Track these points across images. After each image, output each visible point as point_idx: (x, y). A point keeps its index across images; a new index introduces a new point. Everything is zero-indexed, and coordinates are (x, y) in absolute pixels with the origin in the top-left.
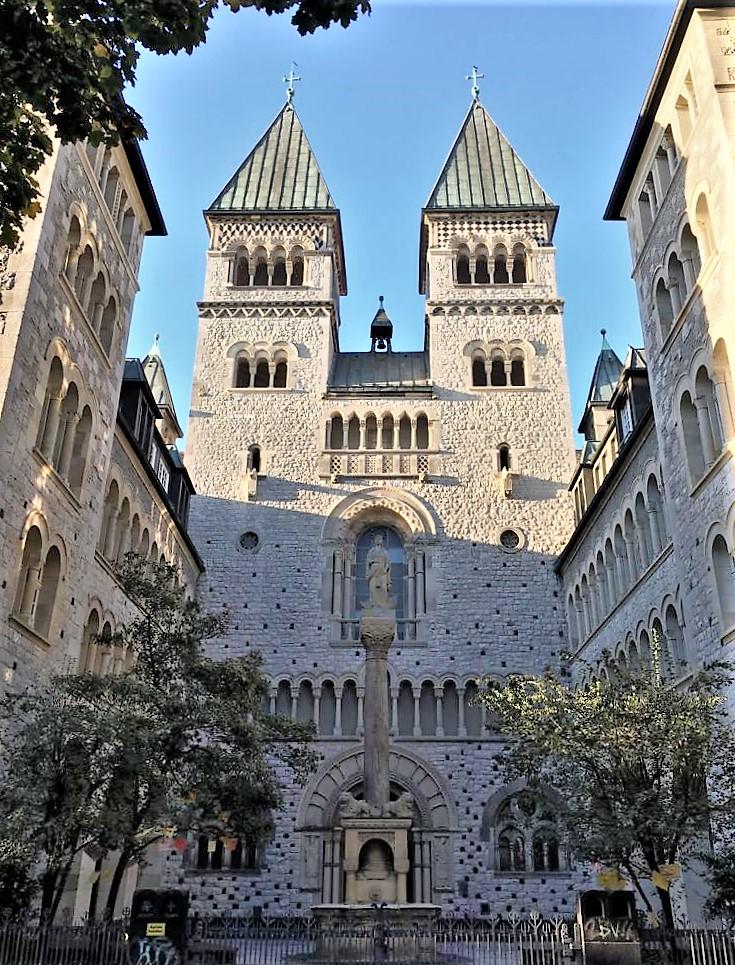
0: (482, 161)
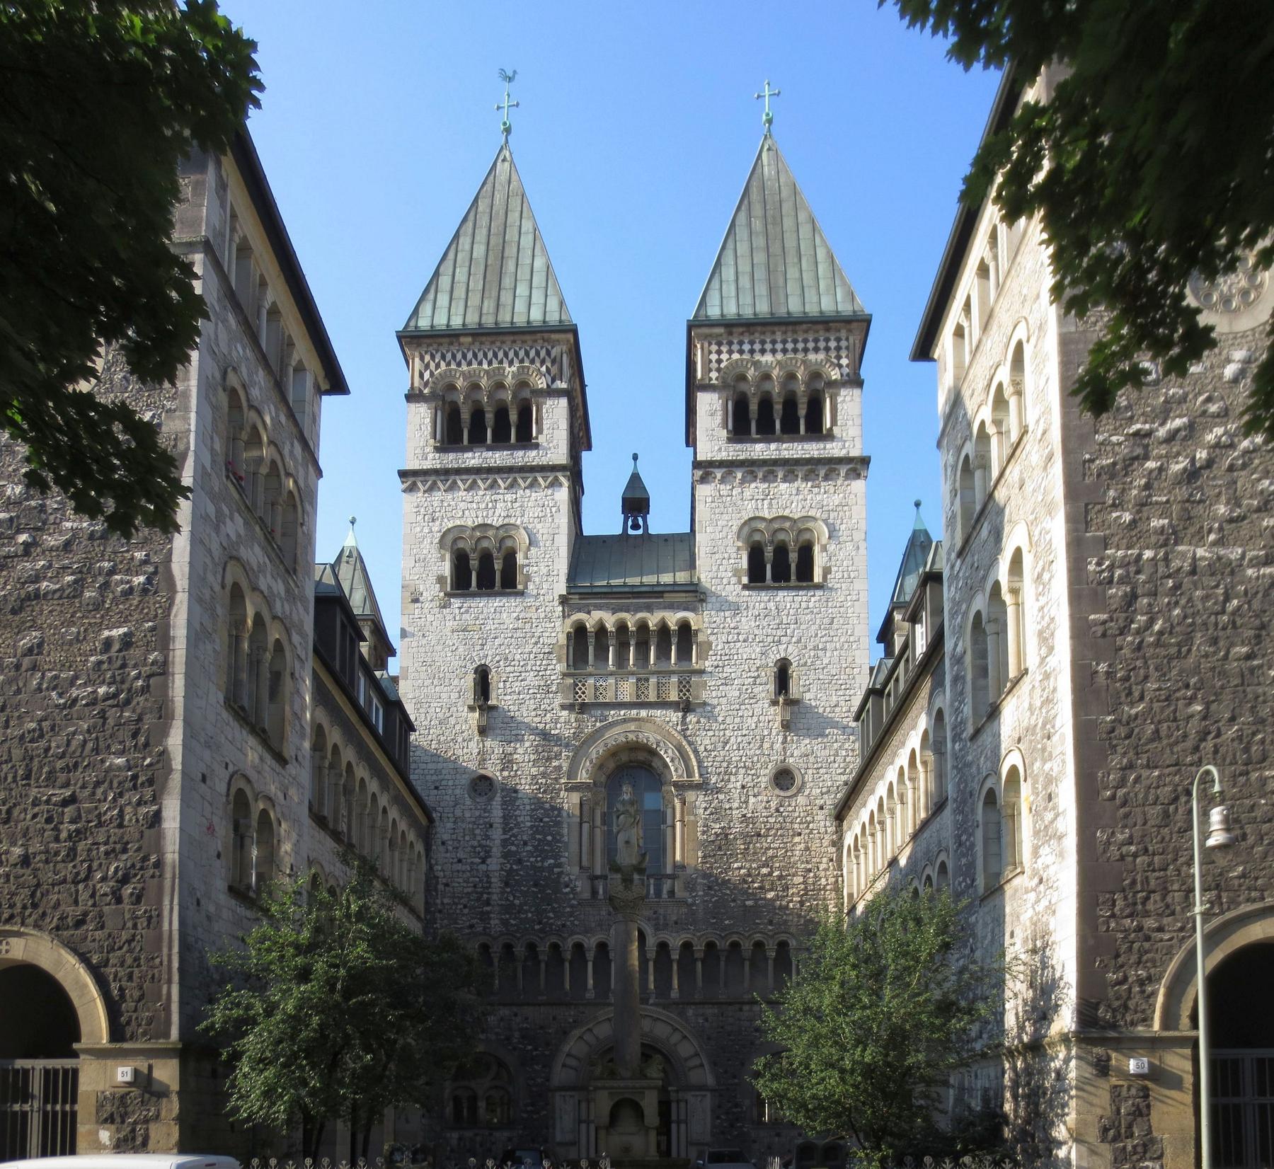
0: (770, 242)
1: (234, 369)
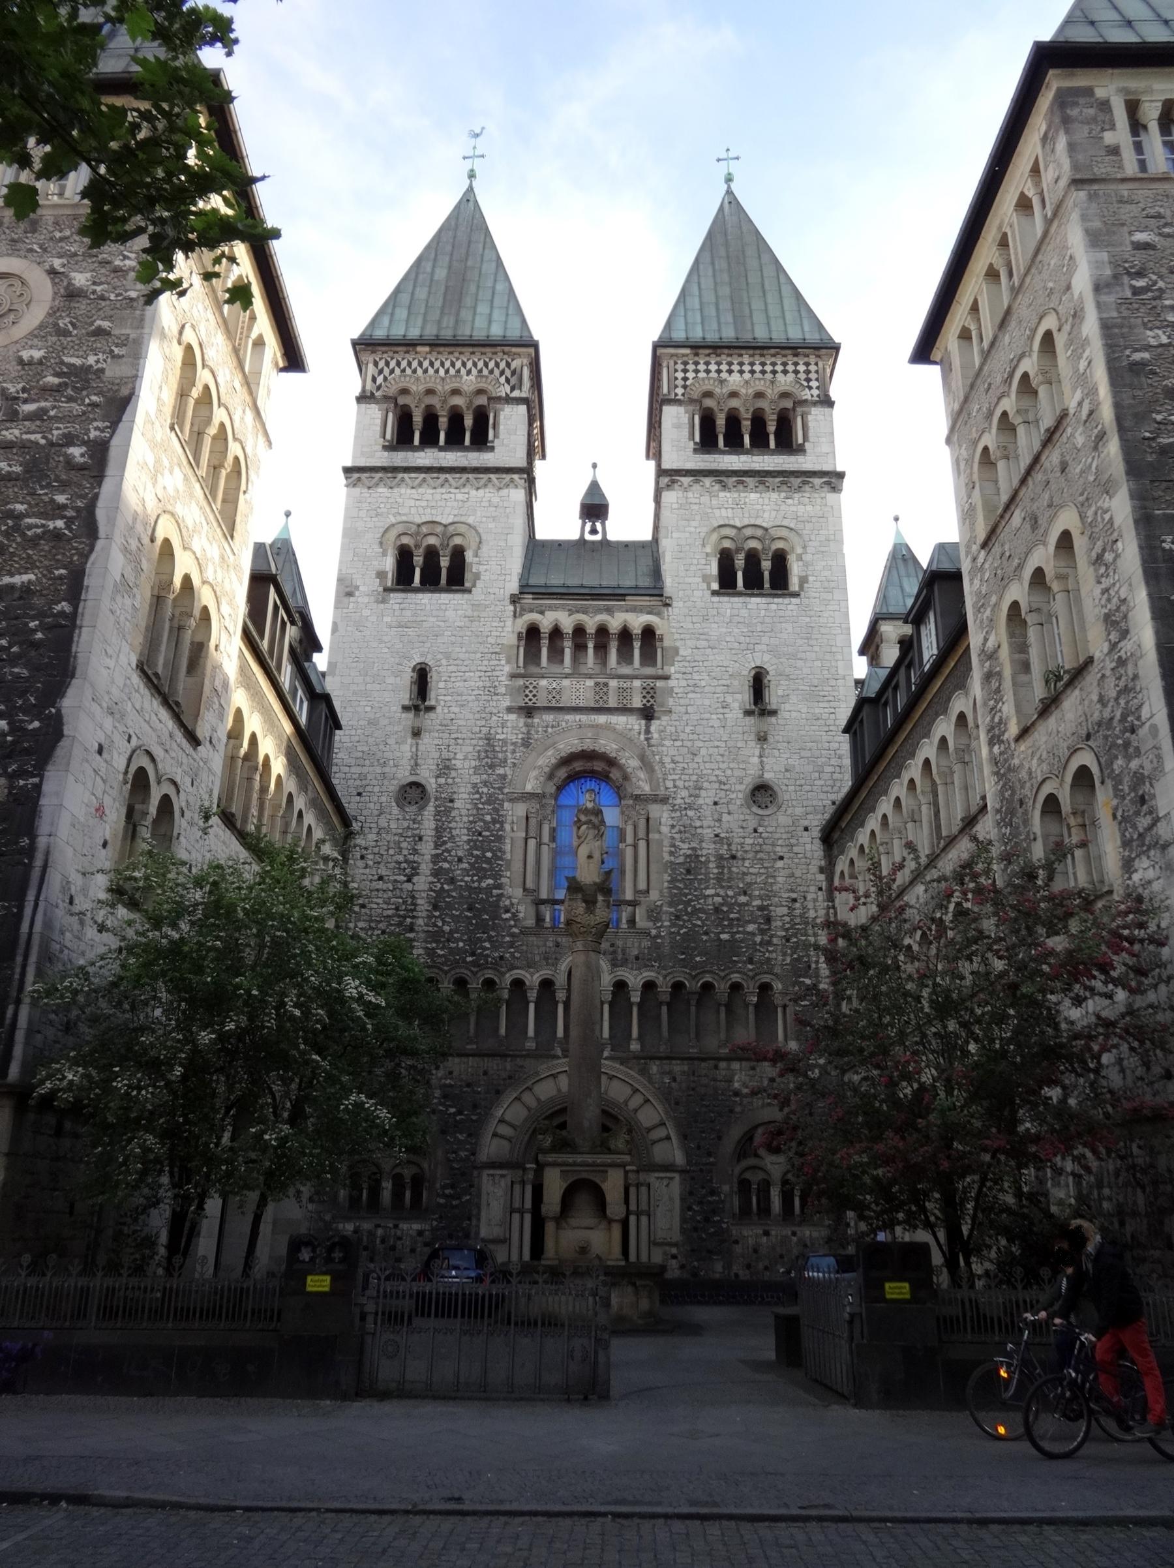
1: (193, 326)
